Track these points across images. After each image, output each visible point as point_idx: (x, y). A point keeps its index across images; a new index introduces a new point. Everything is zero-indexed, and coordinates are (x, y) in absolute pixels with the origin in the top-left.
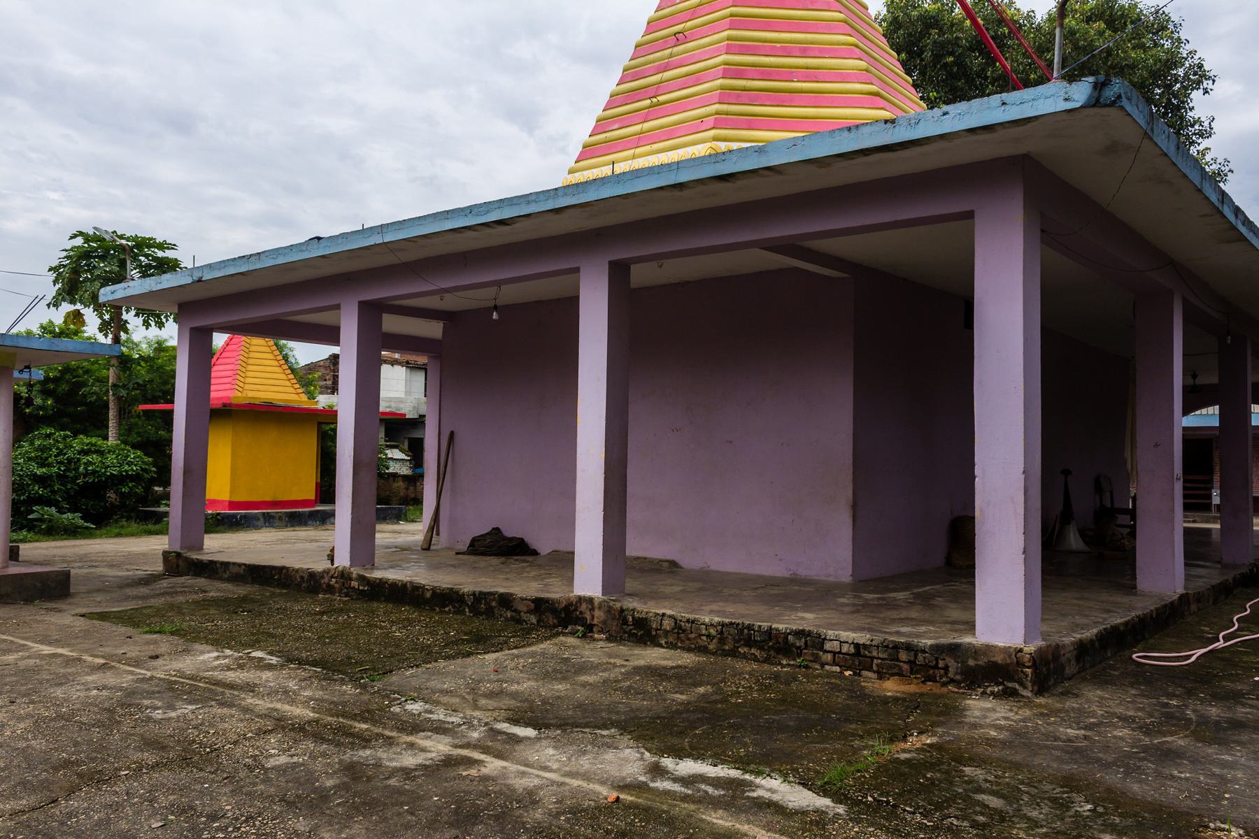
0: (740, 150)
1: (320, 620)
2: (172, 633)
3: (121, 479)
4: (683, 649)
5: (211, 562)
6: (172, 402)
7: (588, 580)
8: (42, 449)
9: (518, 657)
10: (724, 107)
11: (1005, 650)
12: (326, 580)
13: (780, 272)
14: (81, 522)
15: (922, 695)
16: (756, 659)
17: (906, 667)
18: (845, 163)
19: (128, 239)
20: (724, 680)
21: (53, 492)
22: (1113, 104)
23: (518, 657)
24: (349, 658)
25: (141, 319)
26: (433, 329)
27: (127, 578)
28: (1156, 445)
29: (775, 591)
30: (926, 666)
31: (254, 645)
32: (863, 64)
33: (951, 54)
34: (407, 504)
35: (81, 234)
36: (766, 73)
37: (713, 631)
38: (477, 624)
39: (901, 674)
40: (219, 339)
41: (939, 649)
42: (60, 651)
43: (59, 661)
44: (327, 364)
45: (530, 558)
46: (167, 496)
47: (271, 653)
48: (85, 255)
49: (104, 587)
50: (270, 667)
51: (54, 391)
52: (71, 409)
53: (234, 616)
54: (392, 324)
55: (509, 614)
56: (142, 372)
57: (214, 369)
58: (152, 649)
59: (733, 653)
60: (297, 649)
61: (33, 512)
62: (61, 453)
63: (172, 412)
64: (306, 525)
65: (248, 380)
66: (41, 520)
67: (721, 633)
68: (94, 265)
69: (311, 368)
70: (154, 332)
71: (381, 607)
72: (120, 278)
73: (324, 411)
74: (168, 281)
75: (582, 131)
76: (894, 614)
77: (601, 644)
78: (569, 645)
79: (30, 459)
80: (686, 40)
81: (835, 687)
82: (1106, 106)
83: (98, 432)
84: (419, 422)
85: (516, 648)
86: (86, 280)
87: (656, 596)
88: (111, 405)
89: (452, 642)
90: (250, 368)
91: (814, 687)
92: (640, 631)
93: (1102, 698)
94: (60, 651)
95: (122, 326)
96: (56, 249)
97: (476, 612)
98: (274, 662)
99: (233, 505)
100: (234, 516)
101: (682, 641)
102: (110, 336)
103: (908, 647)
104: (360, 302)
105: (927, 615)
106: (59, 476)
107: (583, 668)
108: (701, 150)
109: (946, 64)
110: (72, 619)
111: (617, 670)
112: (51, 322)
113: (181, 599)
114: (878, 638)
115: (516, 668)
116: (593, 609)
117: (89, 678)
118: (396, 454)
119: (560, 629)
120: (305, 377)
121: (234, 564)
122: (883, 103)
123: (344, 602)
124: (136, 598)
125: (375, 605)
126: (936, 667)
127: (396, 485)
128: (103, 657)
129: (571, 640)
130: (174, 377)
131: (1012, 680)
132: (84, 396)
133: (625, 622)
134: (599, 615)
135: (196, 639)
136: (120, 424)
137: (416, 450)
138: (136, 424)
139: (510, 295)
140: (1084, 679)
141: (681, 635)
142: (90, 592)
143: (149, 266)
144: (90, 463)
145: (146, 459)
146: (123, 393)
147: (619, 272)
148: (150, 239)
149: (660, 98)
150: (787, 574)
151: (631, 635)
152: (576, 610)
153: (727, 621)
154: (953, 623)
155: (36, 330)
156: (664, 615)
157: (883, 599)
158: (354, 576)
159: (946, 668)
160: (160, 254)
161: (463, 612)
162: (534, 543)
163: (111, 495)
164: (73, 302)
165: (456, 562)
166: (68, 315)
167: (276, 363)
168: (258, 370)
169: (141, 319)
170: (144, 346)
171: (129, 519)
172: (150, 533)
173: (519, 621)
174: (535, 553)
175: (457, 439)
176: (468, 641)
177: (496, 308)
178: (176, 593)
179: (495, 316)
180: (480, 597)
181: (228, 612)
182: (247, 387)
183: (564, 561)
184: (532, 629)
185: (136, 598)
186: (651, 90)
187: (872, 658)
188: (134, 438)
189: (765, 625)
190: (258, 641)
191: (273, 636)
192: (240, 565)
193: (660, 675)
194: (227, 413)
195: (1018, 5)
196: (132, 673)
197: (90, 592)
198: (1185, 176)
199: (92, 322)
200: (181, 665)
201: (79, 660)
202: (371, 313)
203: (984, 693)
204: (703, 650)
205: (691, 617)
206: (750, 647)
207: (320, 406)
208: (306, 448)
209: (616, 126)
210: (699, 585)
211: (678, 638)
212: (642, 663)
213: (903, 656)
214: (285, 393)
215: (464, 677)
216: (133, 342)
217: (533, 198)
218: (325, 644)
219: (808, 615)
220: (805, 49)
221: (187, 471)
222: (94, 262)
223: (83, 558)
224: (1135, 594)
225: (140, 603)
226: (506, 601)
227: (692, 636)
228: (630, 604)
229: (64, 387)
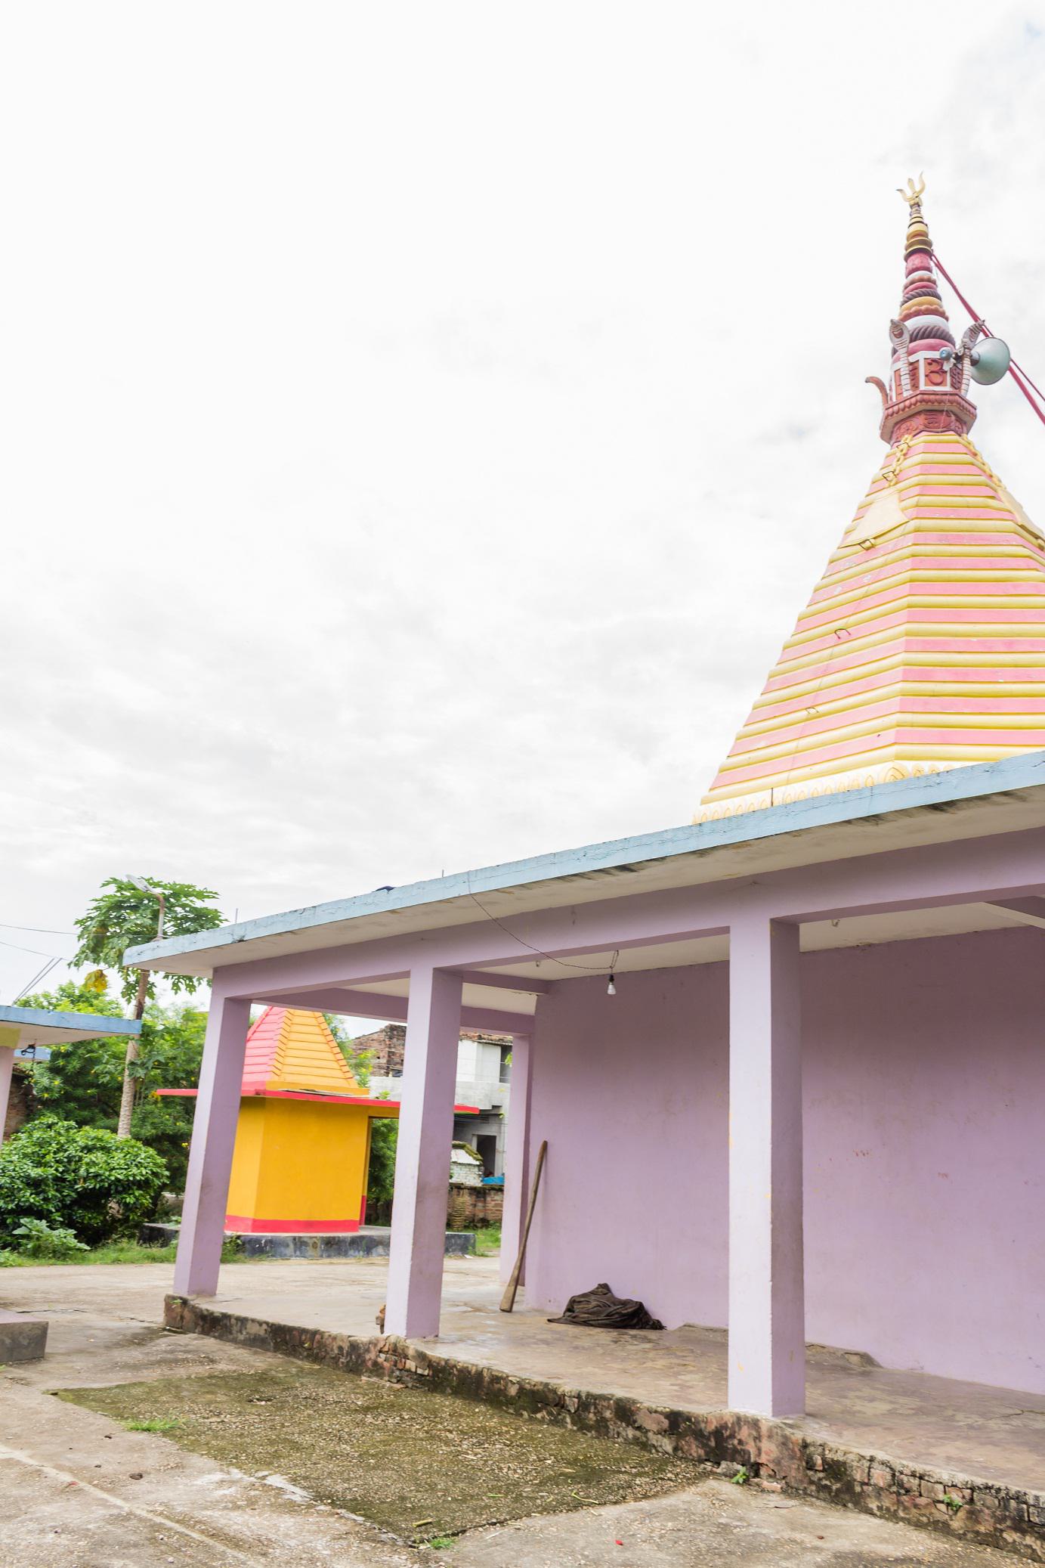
0: (962, 770)
2: (165, 1433)
3: (125, 1186)
4: (908, 1522)
5: (225, 1316)
6: (195, 1085)
7: (747, 1390)
8: (41, 1144)
9: (651, 1515)
10: (908, 717)
12: (372, 1355)
13: (1006, 932)
14: (73, 1242)
19: (165, 887)
21: (46, 1200)
23: (651, 1515)
24: (403, 1499)
25: (170, 981)
26: (524, 1003)
31: (270, 1461)
34: (475, 1228)
35: (115, 880)
37: (956, 1498)
38: (585, 1445)
43: (13, 1473)
44: (382, 1036)
46: (177, 1209)
47: (294, 1481)
48: (118, 906)
50: (292, 1508)
52: (79, 1092)
53: (248, 1408)
54: (474, 995)
56: (165, 1048)
57: (249, 1045)
59: (993, 1540)
61: (20, 1226)
63: (194, 1098)
64: (346, 1255)
65: (288, 1060)
66: (28, 1237)
67: (972, 1501)
68: (126, 919)
69: (363, 1043)
70: (183, 998)
71: (445, 1404)
72: (147, 935)
74: (205, 939)
75: (716, 752)
79: (25, 1156)
84: (491, 1115)
85: (646, 1497)
86: (115, 935)
87: (846, 1420)
89: (550, 1479)
90: (291, 1044)
92: (834, 1483)
96: (85, 902)
97: (583, 1427)
98: (297, 1498)
99: (258, 1225)
100: (258, 1240)
101: (905, 1508)
104: (773, 921)
106: (56, 1179)
108: (879, 773)
112: (71, 983)
115: (648, 1540)
116: (758, 1438)
117: (48, 1509)
118: (460, 1156)
119: (708, 1466)
120: (354, 1054)
121: (253, 1321)
123: (396, 1392)
124: (126, 1366)
125: (438, 1399)
127: (461, 1199)
128: (71, 1470)
130: (201, 1054)
132: (97, 1075)
133: (810, 1466)
136: (134, 1112)
137: (487, 1149)
138: (152, 1112)
139: (629, 961)
141: (903, 1498)
142: (68, 1354)
143: (186, 919)
144: (94, 1164)
146: (141, 1073)
147: (784, 931)
148: (189, 887)
149: (821, 709)
152: (732, 1436)
153: (979, 1481)
155: (54, 992)
156: (872, 1459)
158: (411, 1352)
160: (198, 904)
163: (113, 1207)
164: (96, 961)
165: (548, 1336)
167: (322, 1039)
168: (298, 1048)
169: (170, 981)
170: (170, 1014)
172: (154, 1259)
173: (645, 1446)
174: (658, 1326)
175: (550, 1150)
177: (612, 979)
179: (611, 990)
180: (587, 1402)
182: (286, 1069)
184: (666, 1462)
185: (126, 1366)
186: (808, 701)
188: (148, 1131)
190: (277, 1456)
191: (296, 1447)
194: (255, 1102)
196: (104, 1504)
197: (68, 1354)
199: (116, 982)
200: (171, 1495)
201: (39, 1473)
202: (449, 980)
204: (941, 1528)
205: (920, 1468)
206: (1024, 1532)
207: (372, 1095)
208: (351, 1151)
209: (763, 744)
211: (899, 1502)
214: (327, 1076)
215: (572, 1553)
216: (158, 1010)
217: (669, 836)
218: (370, 1468)
220: (1010, 644)
221: (205, 1187)
222: (125, 913)
226: (625, 1411)
227: (922, 1501)
228: (817, 1433)
229: (75, 1064)
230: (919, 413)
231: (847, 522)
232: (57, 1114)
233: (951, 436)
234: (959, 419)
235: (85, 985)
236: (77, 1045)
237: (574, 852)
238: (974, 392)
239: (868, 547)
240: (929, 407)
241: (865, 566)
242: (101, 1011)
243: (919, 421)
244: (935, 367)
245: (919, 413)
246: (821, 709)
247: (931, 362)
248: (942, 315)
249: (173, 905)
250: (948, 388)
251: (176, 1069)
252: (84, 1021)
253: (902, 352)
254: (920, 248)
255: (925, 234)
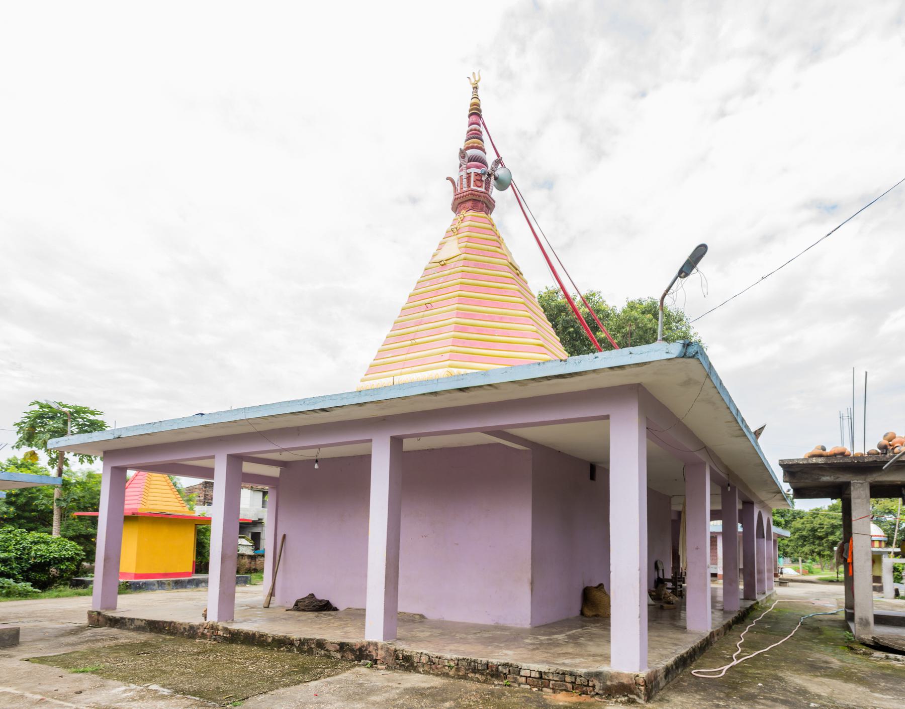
1: (197, 659)
2: (93, 672)
3: (61, 560)
4: (433, 674)
6: (97, 510)
7: (373, 631)
11: (628, 676)
13: (490, 445)
14: (31, 589)
15: (580, 703)
16: (479, 681)
17: (570, 686)
18: (535, 384)
19: (70, 407)
20: (460, 697)
21: (12, 569)
22: (693, 356)
24: (218, 688)
25: (77, 458)
26: (275, 472)
27: (62, 629)
28: (697, 548)
29: (487, 635)
30: (582, 685)
31: (151, 679)
32: (534, 328)
33: (573, 327)
34: (251, 573)
35: (38, 403)
36: (480, 330)
37: (452, 664)
38: (303, 659)
39: (566, 690)
40: (130, 473)
41: (590, 675)
42: (8, 689)
43: (7, 698)
44: (201, 487)
45: (333, 613)
46: (91, 570)
47: (163, 686)
48: (41, 416)
49: (45, 637)
50: (163, 697)
51: (15, 502)
52: (27, 514)
53: (138, 657)
54: (248, 468)
55: (323, 652)
56: (78, 492)
58: (77, 687)
59: (465, 677)
60: (182, 682)
62: (18, 543)
65: (149, 498)
69: (191, 490)
70: (86, 466)
71: (237, 648)
72: (62, 433)
73: (199, 518)
74: (96, 436)
76: (559, 650)
77: (382, 672)
78: (361, 673)
80: (432, 308)
81: (528, 700)
82: (690, 357)
83: (46, 529)
84: (258, 523)
85: (329, 676)
86: (40, 432)
88: (55, 512)
91: (515, 700)
92: (407, 663)
93: (682, 702)
94: (8, 689)
95: (65, 462)
96: (21, 412)
97: (301, 651)
99: (137, 576)
100: (138, 583)
102: (56, 468)
103: (571, 674)
104: (229, 456)
105: (577, 650)
106: (16, 558)
107: (372, 691)
109: (569, 333)
110: (19, 663)
111: (394, 691)
113: (100, 645)
114: (553, 668)
116: (377, 650)
118: (243, 541)
119: (356, 662)
120: (187, 495)
122: (545, 351)
123: (214, 645)
124: (68, 645)
125: (234, 646)
126: (588, 686)
128: (41, 693)
129: (363, 670)
131: (632, 693)
132: (37, 506)
133: (397, 658)
134: (381, 654)
135: (109, 677)
136: (61, 524)
137: (256, 539)
139: (325, 453)
140: (669, 689)
141: (433, 666)
142: (34, 641)
143: (85, 425)
144: (40, 550)
145: (79, 547)
146: (64, 504)
147: (396, 442)
149: (417, 341)
150: (492, 623)
151: (401, 666)
153: (461, 657)
154: (594, 655)
157: (551, 639)
158: (220, 628)
159: (594, 686)
160: (92, 417)
161: (292, 651)
162: (334, 603)
163: (53, 570)
165: (286, 617)
166: (26, 454)
168: (154, 492)
169: (77, 458)
171: (65, 584)
173: (329, 657)
174: (336, 609)
175: (287, 538)
176: (297, 672)
177: (317, 461)
178: (97, 640)
179: (316, 466)
180: (303, 642)
181: (133, 654)
183: (358, 615)
184: (338, 662)
185: (68, 645)
187: (549, 680)
188: (71, 533)
189: (484, 660)
190: (154, 677)
191: (164, 672)
192: (142, 620)
193: (421, 694)
194: (133, 518)
195: (607, 303)
197: (34, 641)
198: (723, 399)
199: (43, 459)
201: (22, 696)
202: (235, 461)
203: (616, 702)
204: (446, 675)
205: (439, 655)
207: (196, 515)
210: (441, 631)
212: (408, 685)
213: (568, 679)
214: (174, 506)
215: (295, 701)
219: (510, 652)
220: (501, 318)
221: (107, 559)
222: (46, 421)
223: (31, 615)
224: (686, 632)
225: (70, 649)
226: (320, 644)
229: (22, 500)
230: (469, 200)
231: (434, 251)
232: (14, 526)
233: (483, 214)
234: (487, 206)
235: (24, 458)
236: (23, 490)
237: (299, 401)
238: (495, 193)
239: (443, 264)
240: (474, 198)
241: (441, 273)
242: (36, 472)
243: (469, 204)
244: (478, 178)
245: (469, 200)
246: (417, 341)
247: (477, 174)
248: (483, 150)
249: (76, 418)
250: (483, 190)
251: (85, 503)
252: (25, 477)
253: (464, 166)
254: (476, 112)
255: (478, 105)
